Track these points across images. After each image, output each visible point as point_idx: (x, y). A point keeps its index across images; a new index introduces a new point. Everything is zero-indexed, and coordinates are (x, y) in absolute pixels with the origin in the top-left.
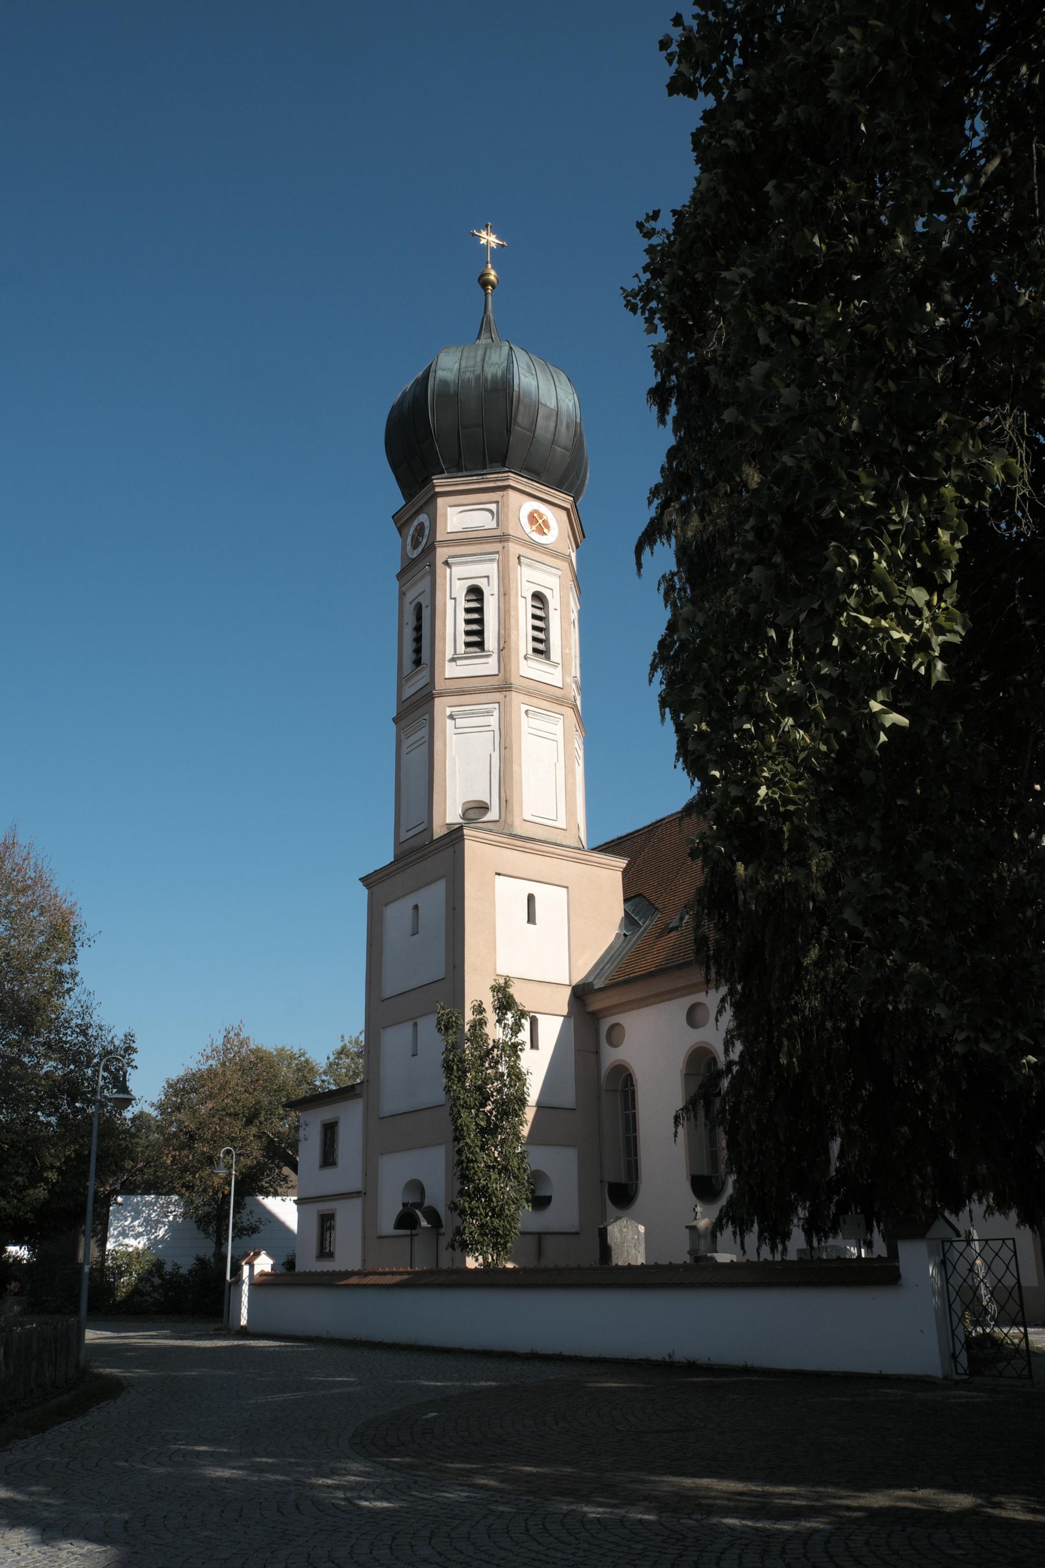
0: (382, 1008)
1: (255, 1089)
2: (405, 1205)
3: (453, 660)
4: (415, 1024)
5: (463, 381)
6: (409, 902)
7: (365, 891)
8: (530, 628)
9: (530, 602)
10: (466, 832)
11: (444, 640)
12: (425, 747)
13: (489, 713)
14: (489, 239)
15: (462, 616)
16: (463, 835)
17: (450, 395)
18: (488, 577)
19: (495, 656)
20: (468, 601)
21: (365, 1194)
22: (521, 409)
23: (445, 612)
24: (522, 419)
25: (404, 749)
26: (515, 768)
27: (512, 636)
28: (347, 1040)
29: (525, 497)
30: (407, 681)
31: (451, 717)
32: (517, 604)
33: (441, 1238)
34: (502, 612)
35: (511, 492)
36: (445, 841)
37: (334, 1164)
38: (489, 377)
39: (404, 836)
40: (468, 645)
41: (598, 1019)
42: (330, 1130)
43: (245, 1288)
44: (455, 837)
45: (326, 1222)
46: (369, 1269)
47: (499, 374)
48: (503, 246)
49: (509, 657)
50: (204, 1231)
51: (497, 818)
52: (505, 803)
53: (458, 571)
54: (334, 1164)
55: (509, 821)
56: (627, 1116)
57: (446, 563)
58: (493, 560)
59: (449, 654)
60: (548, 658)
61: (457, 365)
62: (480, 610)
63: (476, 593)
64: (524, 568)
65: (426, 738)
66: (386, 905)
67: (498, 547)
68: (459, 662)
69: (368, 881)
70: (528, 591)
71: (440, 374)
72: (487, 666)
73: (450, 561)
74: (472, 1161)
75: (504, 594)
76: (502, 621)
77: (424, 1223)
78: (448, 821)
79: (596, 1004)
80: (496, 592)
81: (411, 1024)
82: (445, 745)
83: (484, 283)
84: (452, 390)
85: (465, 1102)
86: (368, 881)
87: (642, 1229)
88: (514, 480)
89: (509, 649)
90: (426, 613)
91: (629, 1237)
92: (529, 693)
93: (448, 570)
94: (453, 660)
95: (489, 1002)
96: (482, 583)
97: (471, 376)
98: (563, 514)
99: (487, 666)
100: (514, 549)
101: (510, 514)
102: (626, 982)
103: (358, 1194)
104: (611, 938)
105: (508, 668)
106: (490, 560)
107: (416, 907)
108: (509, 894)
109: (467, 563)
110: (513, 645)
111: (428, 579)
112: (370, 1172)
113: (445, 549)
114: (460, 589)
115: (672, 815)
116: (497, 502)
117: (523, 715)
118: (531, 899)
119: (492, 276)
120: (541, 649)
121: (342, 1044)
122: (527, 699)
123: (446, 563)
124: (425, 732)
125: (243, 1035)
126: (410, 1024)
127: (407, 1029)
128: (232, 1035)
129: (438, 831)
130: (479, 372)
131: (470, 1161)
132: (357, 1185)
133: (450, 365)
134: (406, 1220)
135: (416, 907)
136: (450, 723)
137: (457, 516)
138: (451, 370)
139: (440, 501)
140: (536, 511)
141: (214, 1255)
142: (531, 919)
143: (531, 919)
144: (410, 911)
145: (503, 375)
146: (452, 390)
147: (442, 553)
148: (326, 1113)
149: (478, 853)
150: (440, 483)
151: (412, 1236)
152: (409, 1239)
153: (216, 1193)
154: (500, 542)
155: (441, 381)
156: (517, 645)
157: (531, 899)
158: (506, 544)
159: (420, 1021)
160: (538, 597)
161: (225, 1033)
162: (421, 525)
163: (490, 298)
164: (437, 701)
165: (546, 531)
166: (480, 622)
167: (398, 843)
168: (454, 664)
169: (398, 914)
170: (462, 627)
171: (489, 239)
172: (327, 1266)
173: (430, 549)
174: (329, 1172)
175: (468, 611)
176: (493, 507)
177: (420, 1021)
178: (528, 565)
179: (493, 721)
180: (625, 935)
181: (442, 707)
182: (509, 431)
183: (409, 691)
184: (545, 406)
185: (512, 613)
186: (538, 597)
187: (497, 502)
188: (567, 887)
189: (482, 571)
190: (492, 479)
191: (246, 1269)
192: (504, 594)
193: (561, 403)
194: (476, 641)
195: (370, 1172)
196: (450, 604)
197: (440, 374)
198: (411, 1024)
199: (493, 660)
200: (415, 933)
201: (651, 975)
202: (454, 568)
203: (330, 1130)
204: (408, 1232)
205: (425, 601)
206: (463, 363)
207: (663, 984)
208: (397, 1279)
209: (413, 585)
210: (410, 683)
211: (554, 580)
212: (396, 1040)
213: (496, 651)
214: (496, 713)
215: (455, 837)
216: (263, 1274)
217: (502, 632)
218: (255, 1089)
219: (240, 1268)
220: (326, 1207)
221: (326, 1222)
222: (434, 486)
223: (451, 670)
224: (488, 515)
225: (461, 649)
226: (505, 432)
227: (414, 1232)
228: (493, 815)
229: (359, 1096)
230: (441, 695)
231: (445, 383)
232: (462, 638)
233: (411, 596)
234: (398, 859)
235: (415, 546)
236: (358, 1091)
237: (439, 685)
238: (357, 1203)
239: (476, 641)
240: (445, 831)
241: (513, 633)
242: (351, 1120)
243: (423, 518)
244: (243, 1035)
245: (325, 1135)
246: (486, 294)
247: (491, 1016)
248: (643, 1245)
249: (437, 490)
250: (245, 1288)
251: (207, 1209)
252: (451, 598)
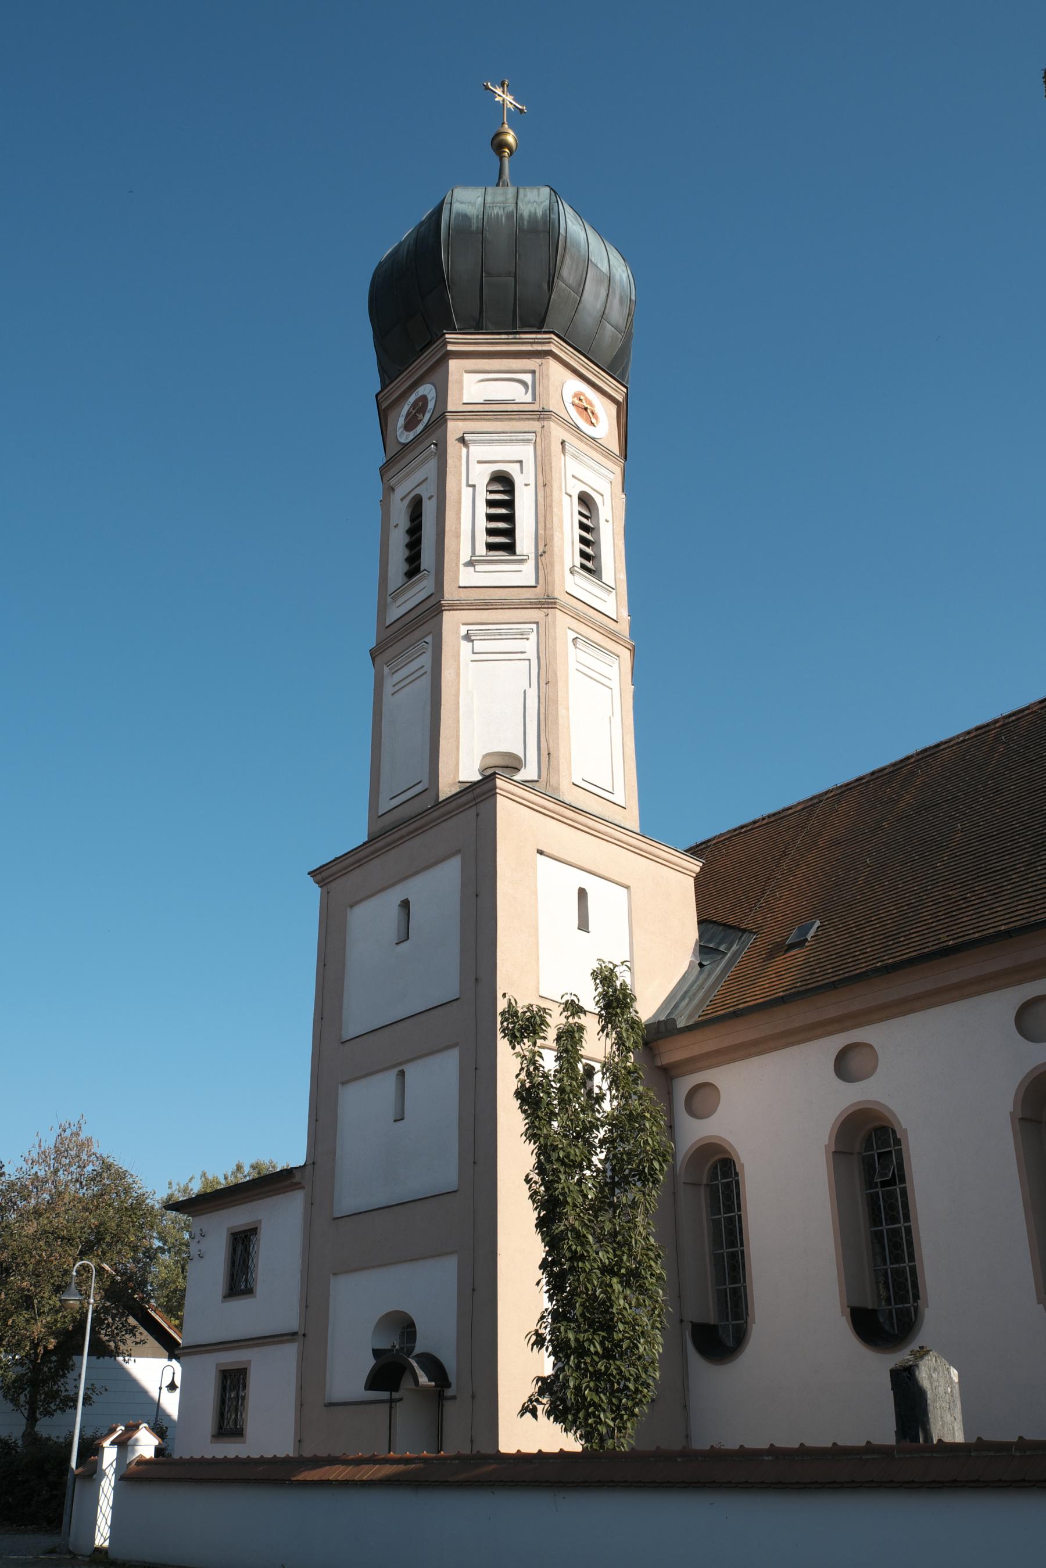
0: (338, 1059)
1: (97, 1207)
2: (376, 1353)
3: (471, 563)
4: (402, 1073)
5: (490, 217)
6: (393, 897)
7: (316, 891)
8: (577, 539)
9: (577, 508)
10: (499, 783)
11: (458, 536)
12: (425, 682)
13: (523, 636)
14: (506, 98)
15: (482, 510)
16: (495, 787)
17: (475, 233)
18: (521, 462)
19: (531, 563)
20: (491, 492)
21: (307, 1337)
22: (568, 261)
23: (459, 502)
24: (568, 272)
25: (388, 688)
26: (562, 712)
27: (556, 539)
28: (175, 1187)
29: (568, 373)
30: (394, 599)
31: (468, 637)
32: (561, 501)
33: (449, 1408)
34: (541, 508)
35: (552, 363)
36: (464, 799)
37: (249, 1291)
38: (526, 215)
39: (384, 806)
40: (490, 547)
41: (672, 1078)
42: (242, 1243)
43: (107, 1488)
44: (480, 794)
45: (232, 1384)
46: (307, 1453)
47: (540, 213)
48: (521, 111)
49: (552, 565)
50: (12, 1401)
51: (536, 778)
52: (547, 757)
53: (477, 451)
54: (249, 1291)
55: (553, 781)
56: (716, 1224)
57: (462, 440)
58: (528, 441)
59: (465, 556)
60: (600, 578)
61: (480, 200)
62: (510, 504)
63: (503, 481)
64: (570, 461)
65: (428, 668)
66: (351, 907)
67: (536, 425)
68: (479, 568)
69: (322, 875)
70: (575, 490)
71: (457, 207)
72: (519, 574)
73: (467, 437)
74: (582, 1258)
75: (544, 485)
76: (541, 519)
77: (423, 1380)
78: (461, 779)
79: (673, 1053)
80: (532, 482)
81: (392, 1075)
82: (458, 674)
83: (499, 146)
84: (474, 227)
85: (568, 1156)
86: (322, 875)
87: (954, 1373)
88: (556, 346)
89: (552, 555)
90: (429, 510)
91: (941, 1390)
92: (577, 617)
93: (464, 450)
94: (471, 563)
95: (589, 997)
96: (513, 470)
97: (501, 212)
98: (613, 408)
99: (519, 574)
100: (557, 432)
101: (551, 388)
102: (736, 1014)
103: (291, 1336)
104: (684, 968)
105: (549, 578)
106: (523, 441)
107: (405, 904)
108: (555, 885)
109: (491, 442)
110: (556, 550)
111: (433, 463)
112: (314, 1301)
113: (460, 424)
114: (481, 476)
115: (722, 835)
116: (533, 372)
117: (570, 644)
118: (582, 893)
119: (510, 138)
120: (590, 562)
121: (170, 1192)
122: (575, 624)
123: (462, 440)
124: (426, 660)
125: (83, 1136)
126: (391, 1076)
127: (388, 1081)
128: (68, 1133)
129: (446, 788)
130: (511, 207)
131: (575, 1257)
132: (290, 1322)
133: (467, 201)
134: (388, 1373)
135: (405, 904)
136: (465, 646)
137: (474, 382)
138: (473, 204)
139: (453, 364)
140: (581, 393)
141: (23, 1436)
142: (583, 925)
143: (583, 925)
144: (393, 911)
145: (544, 214)
146: (474, 227)
147: (454, 428)
148: (238, 1217)
149: (514, 821)
150: (455, 341)
151: (391, 1401)
152: (386, 1407)
153: (35, 1346)
154: (539, 419)
155: (458, 214)
156: (562, 557)
157: (582, 893)
158: (546, 423)
159: (410, 1070)
160: (585, 500)
161: (59, 1131)
162: (424, 399)
163: (506, 161)
164: (447, 616)
165: (594, 421)
166: (510, 518)
167: (374, 815)
168: (471, 569)
169: (372, 919)
170: (482, 524)
171: (506, 98)
172: (230, 1450)
173: (440, 420)
174: (240, 1304)
175: (490, 504)
176: (528, 378)
177: (410, 1070)
178: (575, 457)
179: (530, 646)
180: (701, 965)
181: (453, 624)
182: (551, 286)
183: (395, 612)
184: (596, 266)
185: (555, 510)
186: (585, 500)
187: (533, 372)
188: (627, 887)
189: (515, 455)
190: (528, 341)
191: (110, 1455)
192: (544, 485)
193: (614, 270)
194: (502, 539)
195: (314, 1301)
196: (466, 493)
197: (457, 207)
198: (392, 1075)
199: (529, 568)
200: (405, 936)
201: (782, 1001)
202: (472, 448)
203: (242, 1243)
204: (384, 1395)
205: (426, 492)
206: (489, 199)
207: (801, 1015)
208: (388, 1470)
209: (408, 475)
210: (399, 602)
211: (605, 483)
212: (365, 1101)
213: (532, 556)
214: (533, 637)
215: (480, 794)
216: (142, 1462)
217: (541, 532)
218: (97, 1207)
219: (98, 1451)
220: (231, 1358)
221: (232, 1384)
222: (446, 343)
223: (467, 577)
224: (520, 387)
225: (481, 549)
226: (546, 287)
227: (396, 1395)
228: (529, 772)
229: (298, 1186)
230: (453, 607)
231: (465, 217)
232: (482, 539)
233: (402, 490)
234: (372, 840)
235: (409, 426)
236: (297, 1179)
237: (450, 593)
238: (290, 1351)
239: (502, 539)
240: (455, 790)
241: (557, 536)
242: (281, 1225)
243: (427, 390)
244: (83, 1136)
245: (234, 1250)
246: (501, 158)
247: (591, 1024)
248: (959, 1405)
249: (450, 348)
250: (107, 1488)
251: (20, 1370)
252: (468, 485)
